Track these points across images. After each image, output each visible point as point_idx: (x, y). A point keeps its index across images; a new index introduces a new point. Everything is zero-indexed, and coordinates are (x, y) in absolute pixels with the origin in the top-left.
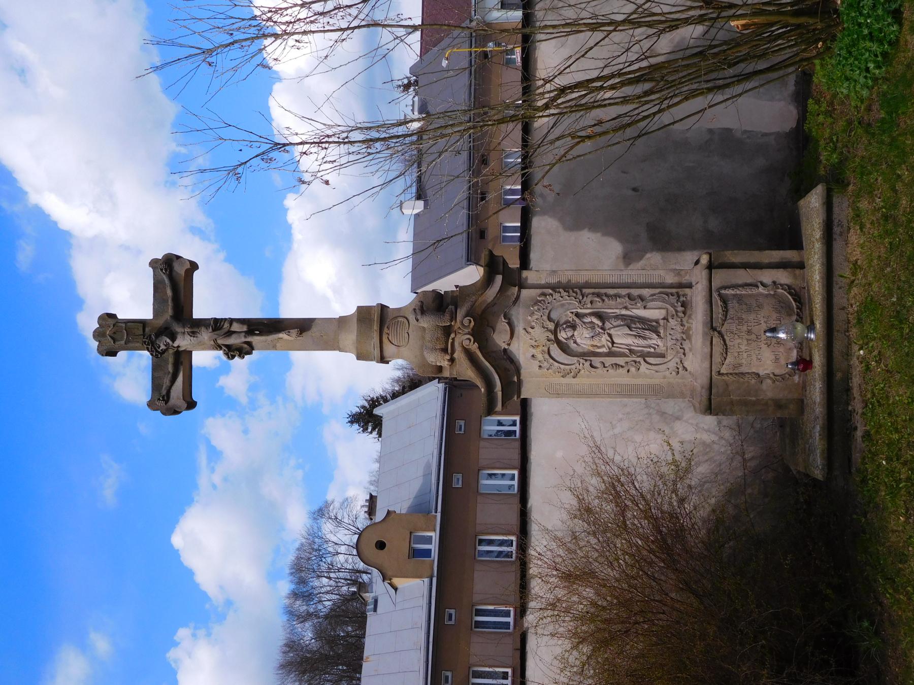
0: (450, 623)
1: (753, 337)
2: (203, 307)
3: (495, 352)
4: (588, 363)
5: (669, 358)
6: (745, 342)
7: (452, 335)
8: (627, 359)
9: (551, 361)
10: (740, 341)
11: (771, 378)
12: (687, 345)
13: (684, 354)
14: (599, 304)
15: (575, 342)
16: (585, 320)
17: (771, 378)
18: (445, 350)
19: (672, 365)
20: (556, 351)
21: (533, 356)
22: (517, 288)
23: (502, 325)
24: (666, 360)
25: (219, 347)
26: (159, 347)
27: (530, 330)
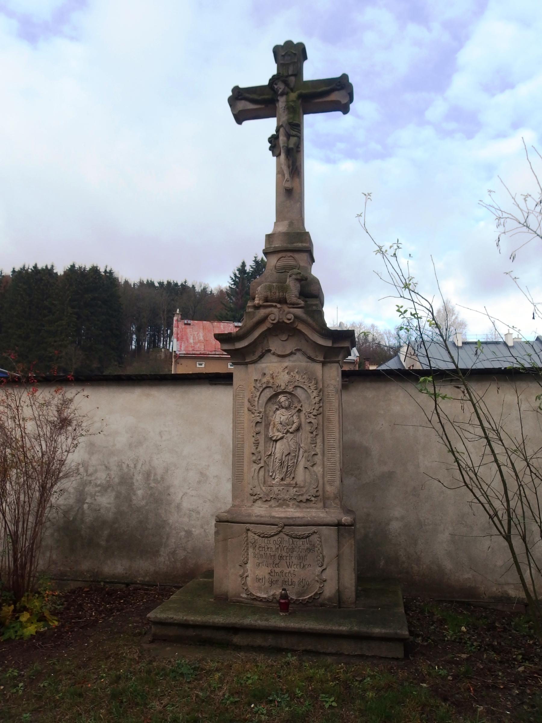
0: (198, 365)
1: (277, 561)
2: (314, 124)
3: (268, 342)
4: (258, 419)
5: (263, 488)
6: (272, 554)
7: (279, 306)
8: (263, 452)
9: (261, 389)
10: (274, 549)
11: (243, 573)
12: (273, 503)
13: (266, 501)
14: (308, 428)
15: (277, 409)
16: (295, 417)
17: (243, 573)
18: (266, 300)
19: (257, 490)
20: (268, 393)
21: (265, 374)
22: (322, 359)
23: (290, 347)
24: (262, 485)
25: (278, 130)
26: (276, 84)
27: (287, 371)
